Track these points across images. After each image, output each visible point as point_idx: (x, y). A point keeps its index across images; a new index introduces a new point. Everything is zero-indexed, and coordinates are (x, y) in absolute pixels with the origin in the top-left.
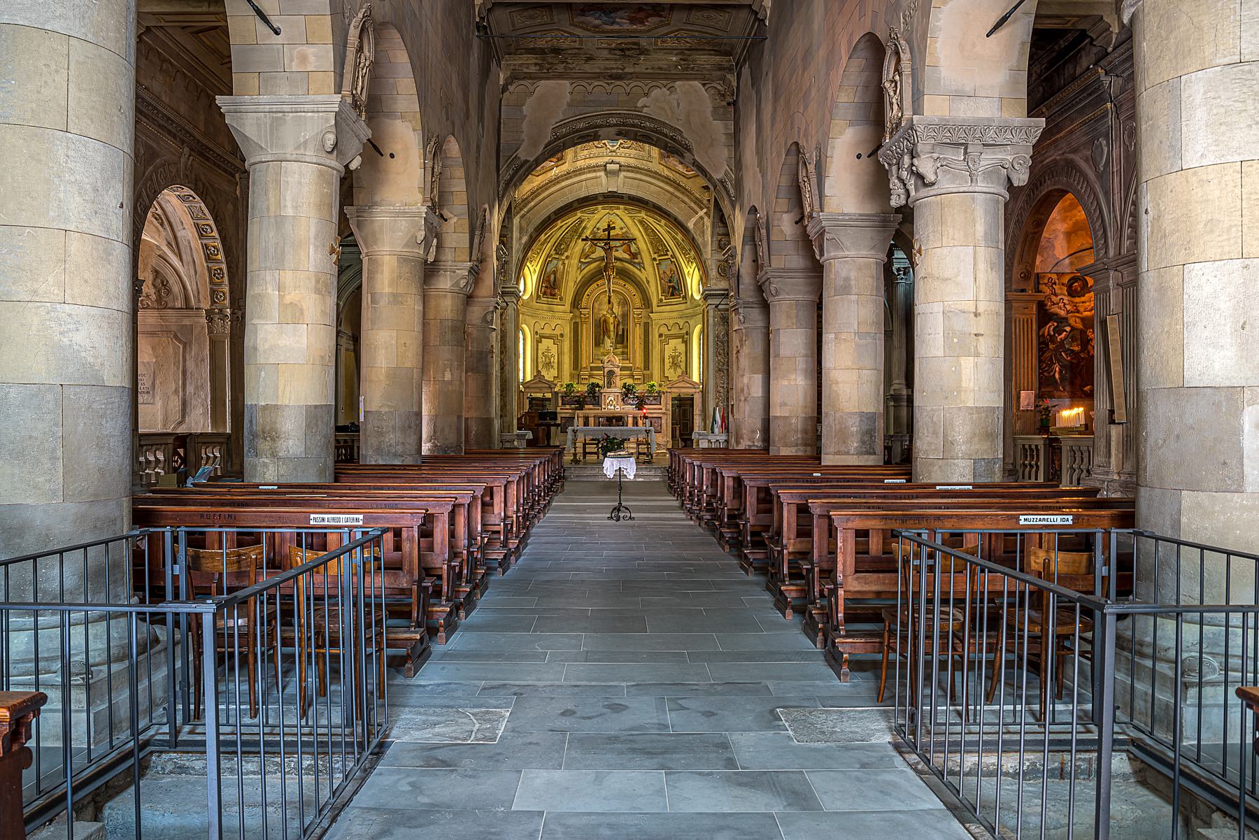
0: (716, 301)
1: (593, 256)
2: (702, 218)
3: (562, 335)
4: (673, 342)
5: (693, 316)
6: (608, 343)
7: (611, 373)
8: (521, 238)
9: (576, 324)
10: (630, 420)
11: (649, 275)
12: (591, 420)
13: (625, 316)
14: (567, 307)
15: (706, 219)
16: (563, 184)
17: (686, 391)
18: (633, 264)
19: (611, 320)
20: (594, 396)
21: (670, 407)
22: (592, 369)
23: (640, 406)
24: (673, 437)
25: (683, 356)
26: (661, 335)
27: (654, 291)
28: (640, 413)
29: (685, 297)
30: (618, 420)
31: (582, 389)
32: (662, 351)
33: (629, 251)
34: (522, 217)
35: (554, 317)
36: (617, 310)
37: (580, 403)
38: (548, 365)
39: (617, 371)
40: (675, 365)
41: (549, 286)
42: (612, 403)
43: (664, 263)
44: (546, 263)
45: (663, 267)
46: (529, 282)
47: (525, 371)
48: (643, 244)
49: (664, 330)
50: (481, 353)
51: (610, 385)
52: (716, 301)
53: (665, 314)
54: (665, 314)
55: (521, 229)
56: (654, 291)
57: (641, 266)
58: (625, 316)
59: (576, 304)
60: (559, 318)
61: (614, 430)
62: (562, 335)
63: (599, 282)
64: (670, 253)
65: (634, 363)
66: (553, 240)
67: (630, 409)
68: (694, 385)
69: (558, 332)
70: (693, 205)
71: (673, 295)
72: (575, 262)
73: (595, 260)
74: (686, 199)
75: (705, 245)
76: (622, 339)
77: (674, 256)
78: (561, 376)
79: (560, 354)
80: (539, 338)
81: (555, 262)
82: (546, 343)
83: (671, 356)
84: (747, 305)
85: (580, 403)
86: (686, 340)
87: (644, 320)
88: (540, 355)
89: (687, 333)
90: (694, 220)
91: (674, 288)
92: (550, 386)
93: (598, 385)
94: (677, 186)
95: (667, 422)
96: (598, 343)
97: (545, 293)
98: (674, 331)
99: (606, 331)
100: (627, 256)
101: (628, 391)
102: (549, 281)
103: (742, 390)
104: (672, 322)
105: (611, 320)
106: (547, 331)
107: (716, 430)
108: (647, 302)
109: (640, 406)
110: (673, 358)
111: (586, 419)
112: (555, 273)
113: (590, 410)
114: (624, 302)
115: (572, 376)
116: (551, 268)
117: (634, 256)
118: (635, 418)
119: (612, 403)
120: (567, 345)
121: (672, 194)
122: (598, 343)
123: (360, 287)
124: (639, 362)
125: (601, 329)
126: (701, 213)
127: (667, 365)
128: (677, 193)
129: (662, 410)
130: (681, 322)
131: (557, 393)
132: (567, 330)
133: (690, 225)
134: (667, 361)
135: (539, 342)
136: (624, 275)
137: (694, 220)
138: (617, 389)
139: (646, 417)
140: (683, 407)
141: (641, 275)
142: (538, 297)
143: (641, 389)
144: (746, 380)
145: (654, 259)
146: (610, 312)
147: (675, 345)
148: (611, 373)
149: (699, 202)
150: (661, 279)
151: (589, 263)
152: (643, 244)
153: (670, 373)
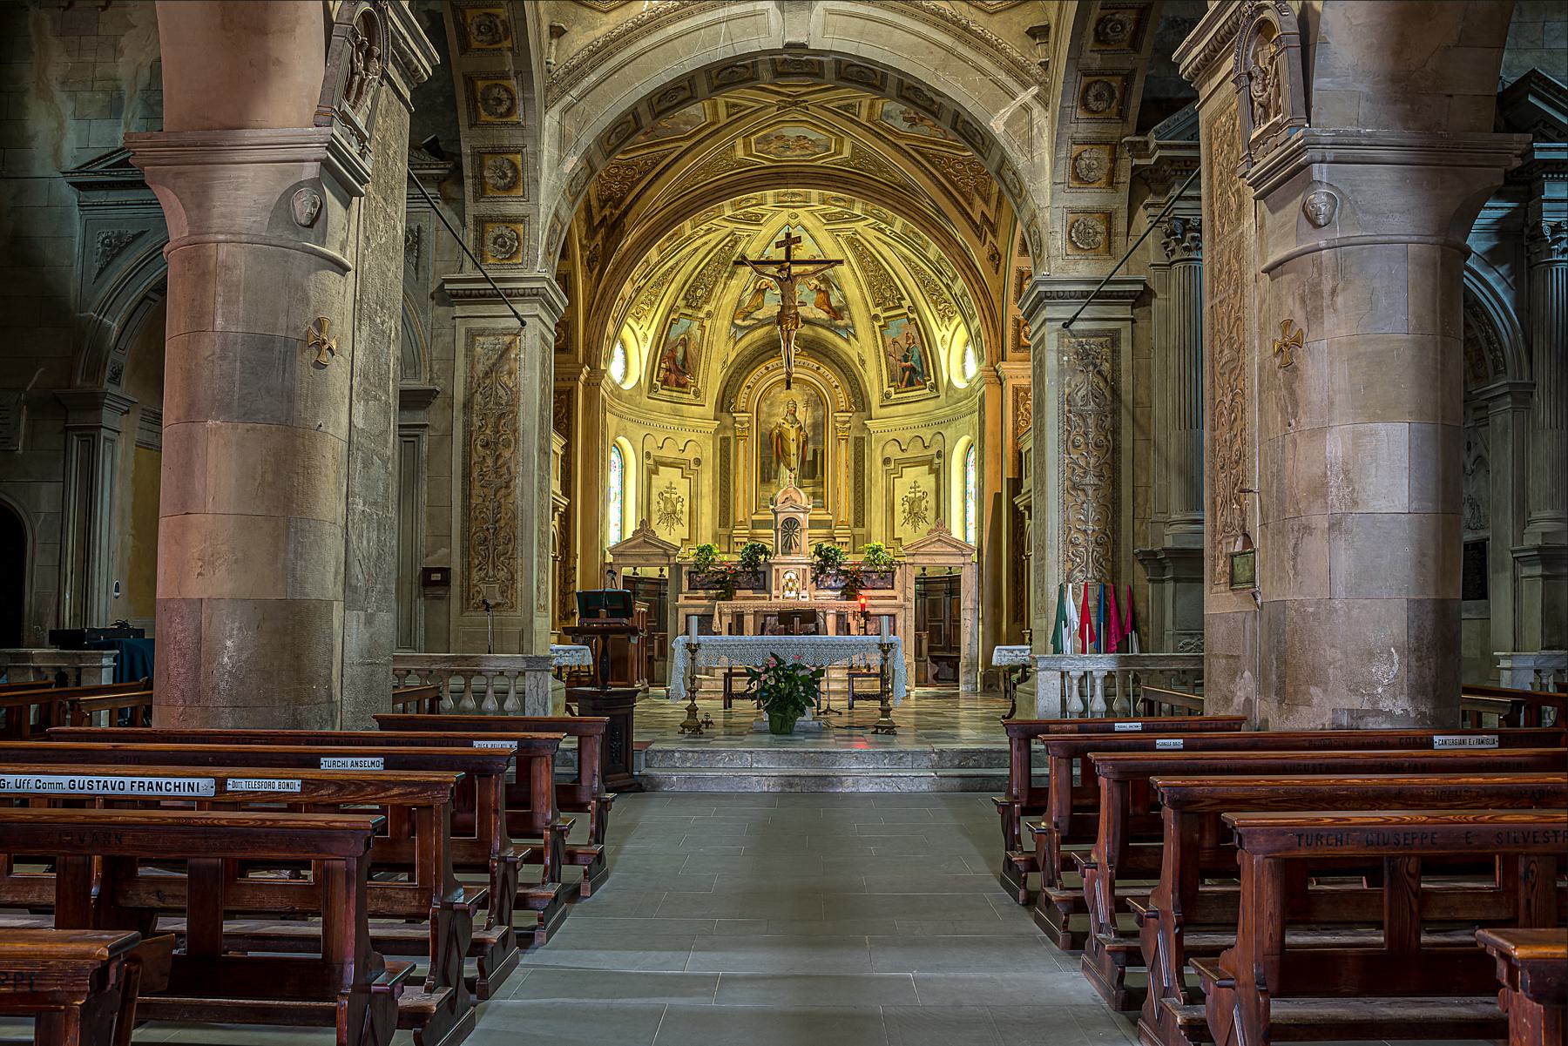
0: (1066, 312)
1: (760, 315)
2: (1026, 108)
3: (698, 462)
4: (911, 474)
5: (950, 421)
6: (786, 476)
7: (791, 524)
8: (561, 161)
9: (725, 440)
10: (831, 621)
11: (865, 349)
12: (749, 621)
13: (819, 426)
14: (709, 409)
15: (1037, 110)
16: (671, 30)
17: (939, 562)
18: (834, 329)
19: (793, 434)
20: (755, 572)
21: (911, 594)
22: (755, 524)
23: (850, 592)
24: (918, 653)
25: (931, 498)
26: (886, 461)
27: (874, 378)
28: (853, 606)
29: (935, 387)
30: (807, 619)
31: (731, 558)
32: (890, 491)
33: (825, 303)
34: (566, 110)
35: (682, 427)
36: (804, 415)
37: (726, 585)
38: (671, 516)
39: (803, 518)
40: (915, 515)
41: (674, 367)
42: (792, 583)
43: (893, 324)
44: (668, 324)
45: (892, 333)
46: (629, 359)
47: (618, 521)
48: (851, 284)
49: (893, 451)
50: (266, 342)
51: (788, 548)
52: (1066, 312)
53: (895, 421)
54: (895, 421)
55: (563, 142)
56: (874, 378)
57: (849, 332)
58: (819, 426)
59: (725, 403)
60: (692, 428)
61: (794, 647)
62: (698, 462)
63: (771, 364)
64: (907, 303)
65: (836, 514)
66: (680, 278)
67: (827, 599)
68: (960, 548)
69: (690, 455)
70: (1002, 76)
71: (910, 383)
72: (723, 323)
73: (762, 323)
74: (986, 63)
75: (1036, 172)
76: (812, 470)
77: (914, 308)
78: (691, 530)
79: (694, 496)
80: (653, 464)
81: (685, 322)
82: (668, 475)
83: (906, 500)
84: (1349, 152)
85: (726, 585)
86: (937, 466)
87: (854, 433)
88: (655, 497)
89: (939, 455)
90: (1006, 112)
91: (914, 370)
92: (667, 551)
93: (763, 550)
94: (963, 31)
95: (907, 622)
96: (767, 476)
97: (665, 382)
98: (915, 451)
99: (782, 455)
100: (824, 316)
101: (825, 562)
102: (674, 359)
103: (1319, 490)
104: (908, 435)
105: (793, 434)
106: (669, 453)
107: (1067, 644)
108: (860, 401)
109: (850, 592)
110: (912, 502)
111: (739, 617)
112: (685, 343)
113: (747, 601)
114: (817, 401)
115: (716, 537)
116: (677, 333)
117: (836, 313)
118: (840, 616)
119: (792, 583)
120: (707, 480)
121: (950, 51)
122: (767, 476)
123: (161, 288)
124: (845, 510)
125: (772, 451)
126: (1026, 96)
127: (899, 517)
128: (962, 49)
129: (898, 602)
130: (927, 435)
131: (679, 567)
132: (708, 452)
133: (997, 125)
134: (898, 508)
135: (653, 471)
136: (816, 349)
137: (1006, 112)
138: (805, 553)
139: (866, 615)
140: (938, 596)
141: (851, 350)
142: (652, 387)
143: (850, 560)
144: (1335, 446)
145: (876, 317)
146: (787, 411)
147: (917, 478)
148: (791, 524)
149: (1019, 72)
150: (888, 355)
151: (751, 328)
152: (851, 284)
153: (905, 532)
